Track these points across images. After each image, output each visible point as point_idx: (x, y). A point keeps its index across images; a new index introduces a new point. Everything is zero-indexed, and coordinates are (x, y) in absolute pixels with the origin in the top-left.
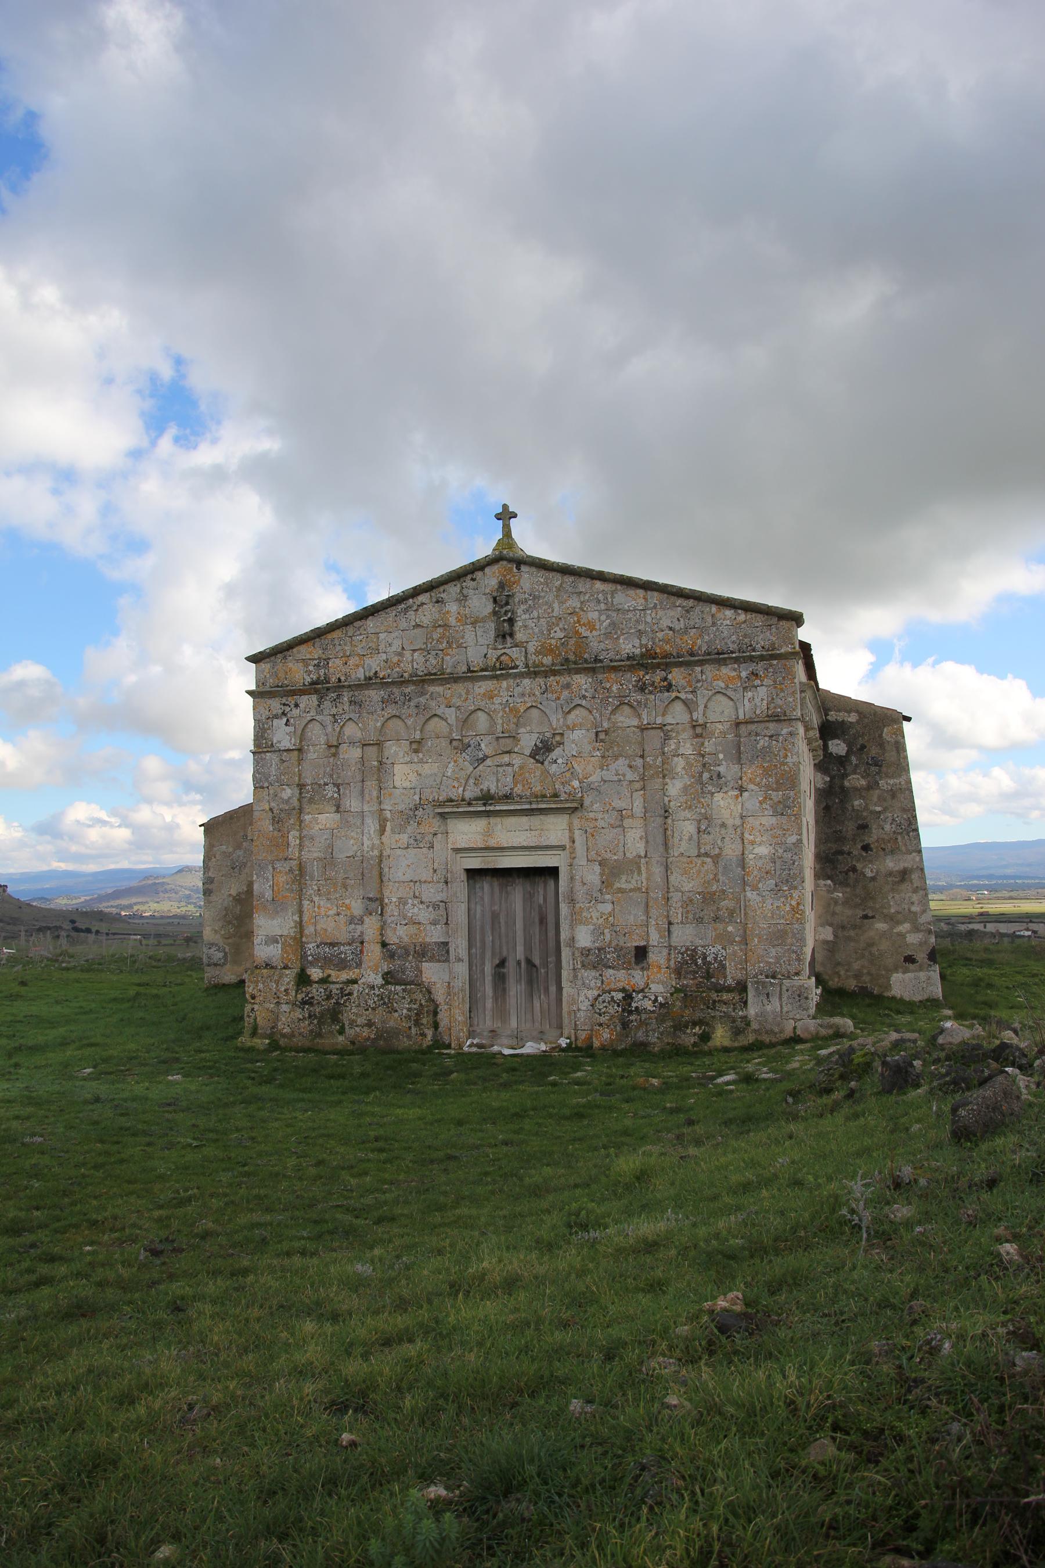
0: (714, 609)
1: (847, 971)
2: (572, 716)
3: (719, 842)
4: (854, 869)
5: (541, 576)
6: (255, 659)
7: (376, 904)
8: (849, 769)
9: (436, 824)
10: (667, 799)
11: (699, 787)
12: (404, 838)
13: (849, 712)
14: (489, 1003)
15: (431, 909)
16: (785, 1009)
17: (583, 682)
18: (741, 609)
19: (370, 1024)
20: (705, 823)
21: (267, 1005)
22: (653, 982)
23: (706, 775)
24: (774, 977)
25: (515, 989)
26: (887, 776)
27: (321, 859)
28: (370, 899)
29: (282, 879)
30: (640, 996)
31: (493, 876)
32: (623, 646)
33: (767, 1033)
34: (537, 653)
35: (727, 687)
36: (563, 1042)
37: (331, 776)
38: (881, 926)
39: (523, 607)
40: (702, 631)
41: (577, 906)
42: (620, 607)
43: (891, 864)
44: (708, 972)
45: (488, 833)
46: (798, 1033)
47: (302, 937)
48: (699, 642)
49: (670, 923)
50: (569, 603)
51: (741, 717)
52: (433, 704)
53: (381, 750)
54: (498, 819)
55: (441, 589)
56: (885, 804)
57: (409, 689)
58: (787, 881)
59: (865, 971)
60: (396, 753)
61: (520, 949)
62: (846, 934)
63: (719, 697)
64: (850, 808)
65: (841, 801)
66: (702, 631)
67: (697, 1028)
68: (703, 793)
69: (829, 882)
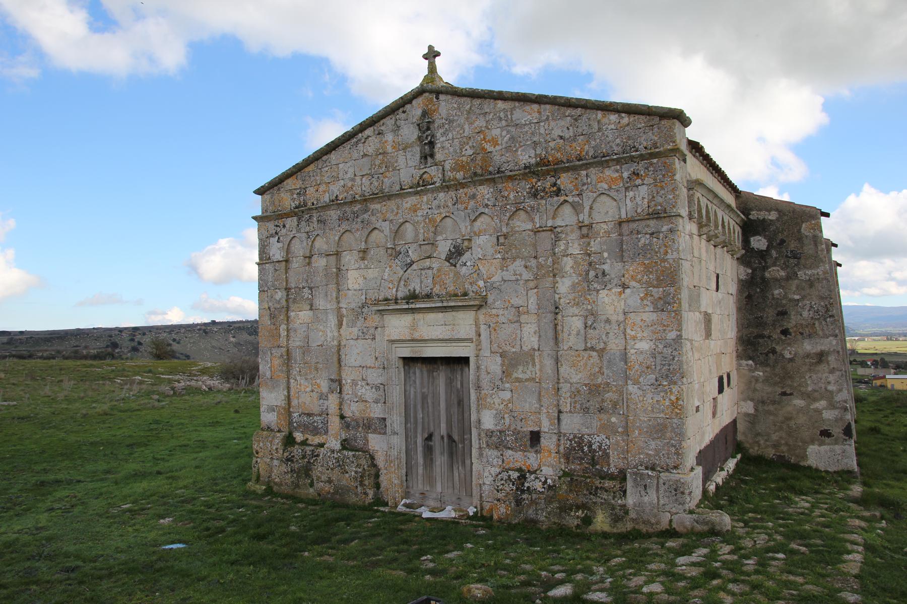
0: (600, 114)
1: (766, 441)
2: (478, 223)
3: (604, 337)
4: (774, 351)
5: (454, 101)
6: (260, 191)
7: (337, 384)
8: (770, 261)
9: (377, 318)
10: (557, 296)
11: (585, 285)
12: (355, 331)
13: (769, 211)
14: (421, 470)
15: (374, 390)
16: (662, 502)
17: (486, 192)
18: (625, 113)
19: (330, 481)
20: (591, 319)
21: (265, 459)
22: (545, 465)
23: (592, 274)
24: (653, 469)
25: (441, 460)
26: (805, 267)
27: (301, 347)
28: (332, 380)
29: (277, 362)
30: (533, 477)
31: (422, 363)
32: (521, 158)
33: (644, 523)
34: (453, 169)
35: (610, 188)
36: (471, 511)
37: (307, 281)
38: (799, 402)
39: (441, 131)
40: (589, 136)
41: (483, 392)
42: (518, 122)
43: (808, 346)
44: (593, 459)
45: (414, 327)
46: (674, 526)
47: (289, 407)
48: (586, 147)
49: (560, 412)
50: (477, 123)
51: (624, 216)
52: (373, 219)
53: (338, 260)
54: (421, 315)
55: (382, 122)
56: (803, 293)
57: (357, 207)
58: (667, 376)
59: (783, 442)
60: (349, 261)
61: (443, 426)
62: (766, 408)
63: (603, 198)
64: (770, 297)
65: (762, 290)
66: (589, 136)
67: (580, 512)
68: (589, 290)
69: (750, 362)
